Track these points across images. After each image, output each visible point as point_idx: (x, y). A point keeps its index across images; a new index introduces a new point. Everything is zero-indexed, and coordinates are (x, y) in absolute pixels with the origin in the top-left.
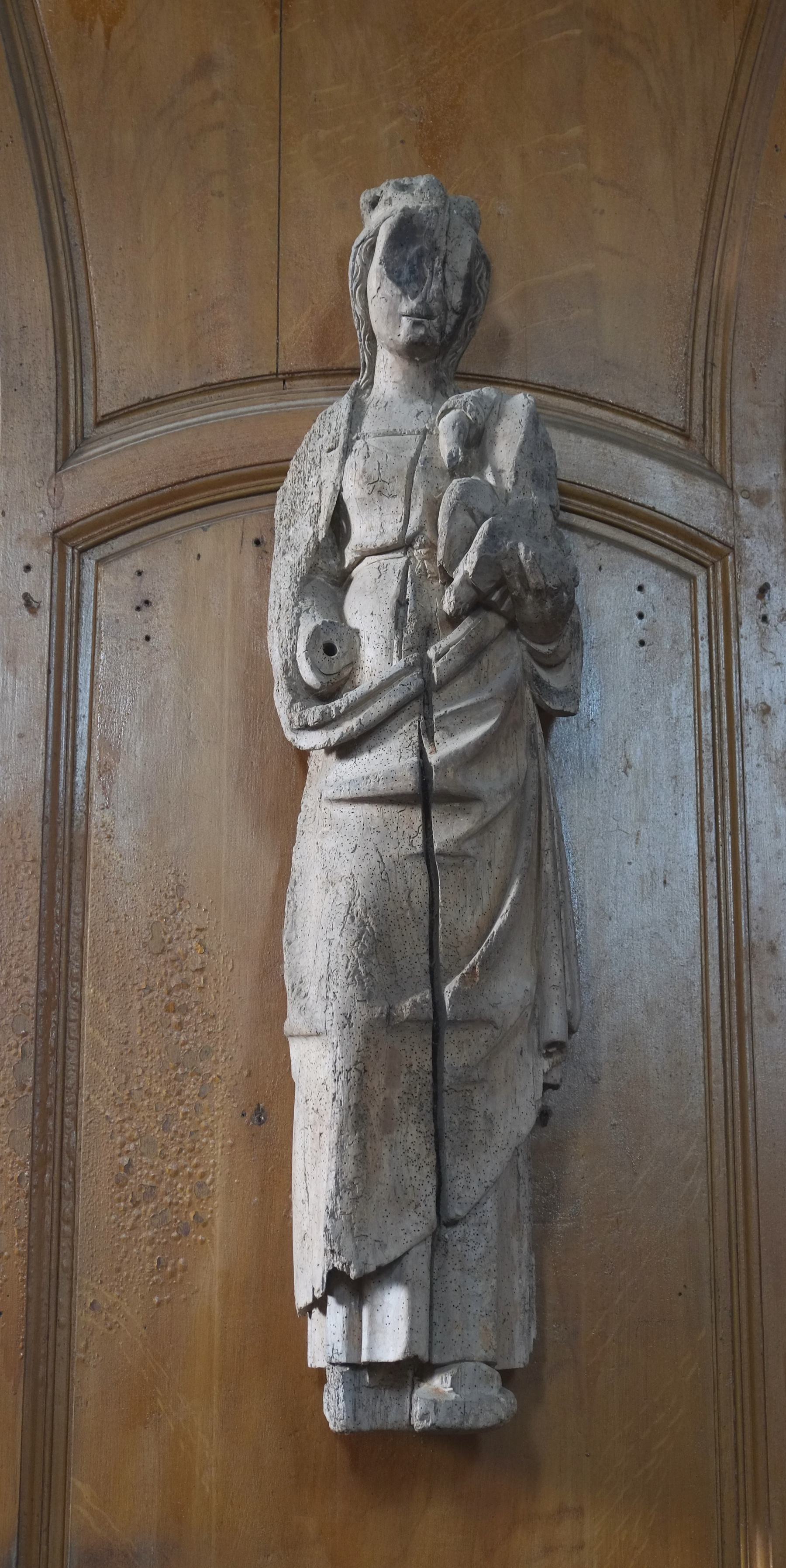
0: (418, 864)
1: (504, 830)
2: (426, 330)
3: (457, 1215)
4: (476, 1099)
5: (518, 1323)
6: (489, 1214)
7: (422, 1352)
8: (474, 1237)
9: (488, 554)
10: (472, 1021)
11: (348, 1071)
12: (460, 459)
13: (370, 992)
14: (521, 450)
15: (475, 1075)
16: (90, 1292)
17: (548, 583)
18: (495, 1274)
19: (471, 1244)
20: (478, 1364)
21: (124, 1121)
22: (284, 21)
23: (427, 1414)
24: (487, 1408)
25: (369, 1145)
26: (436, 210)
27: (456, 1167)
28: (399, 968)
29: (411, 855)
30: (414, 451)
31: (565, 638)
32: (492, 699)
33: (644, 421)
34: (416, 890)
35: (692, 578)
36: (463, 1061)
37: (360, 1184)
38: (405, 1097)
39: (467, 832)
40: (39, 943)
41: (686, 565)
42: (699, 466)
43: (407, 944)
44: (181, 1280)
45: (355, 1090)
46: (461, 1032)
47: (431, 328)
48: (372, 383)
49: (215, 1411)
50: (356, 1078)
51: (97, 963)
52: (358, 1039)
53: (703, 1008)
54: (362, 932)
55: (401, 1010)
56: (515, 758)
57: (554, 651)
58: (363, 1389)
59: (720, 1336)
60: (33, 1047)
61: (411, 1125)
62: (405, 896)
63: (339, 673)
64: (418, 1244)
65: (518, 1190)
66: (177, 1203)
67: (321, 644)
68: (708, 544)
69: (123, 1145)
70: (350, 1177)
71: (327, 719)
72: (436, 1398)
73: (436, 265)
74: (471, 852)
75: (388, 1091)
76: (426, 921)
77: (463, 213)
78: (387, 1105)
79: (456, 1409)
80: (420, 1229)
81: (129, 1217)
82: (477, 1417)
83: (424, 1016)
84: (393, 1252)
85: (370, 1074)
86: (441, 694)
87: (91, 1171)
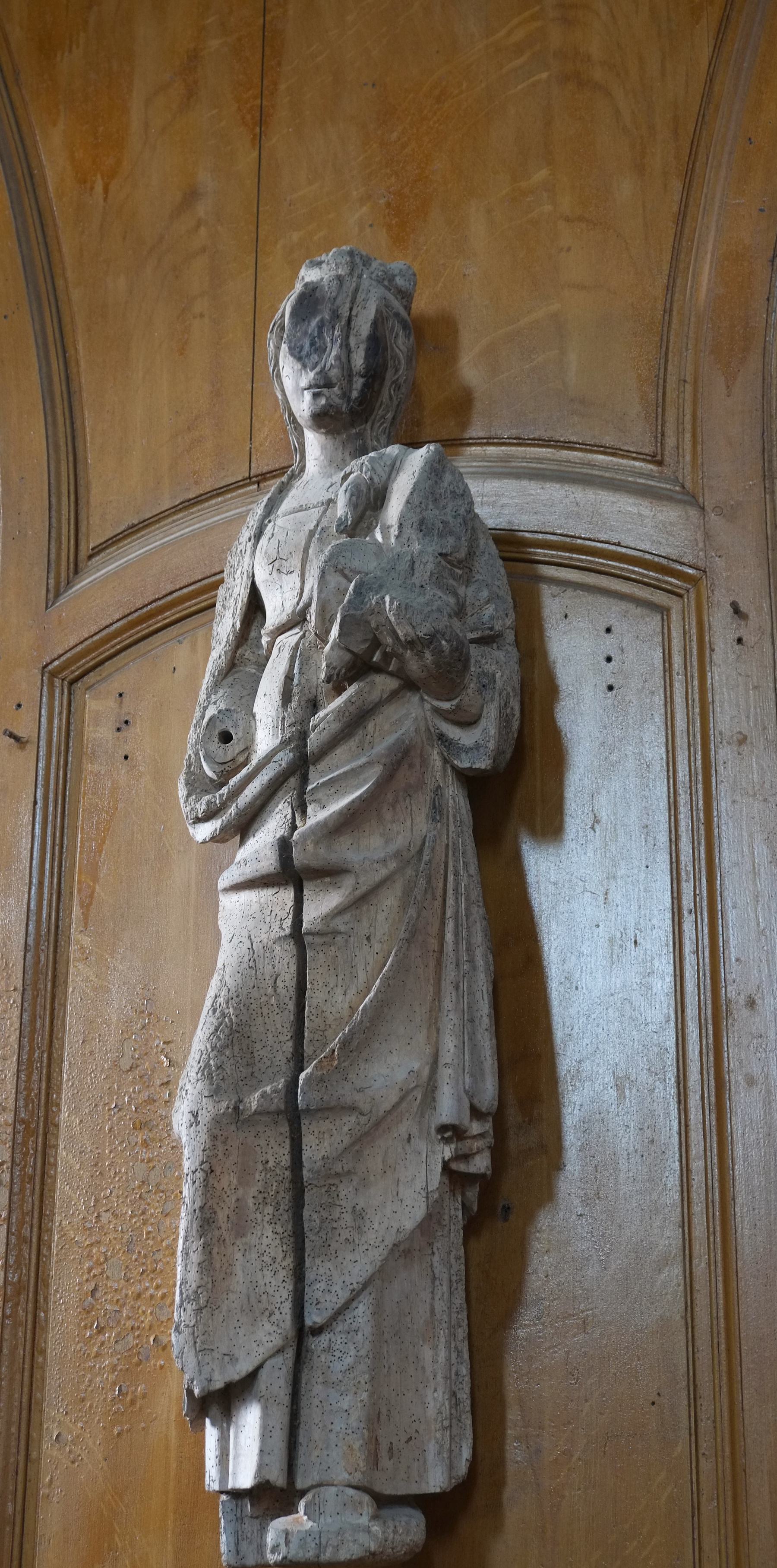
0: (286, 947)
1: (389, 900)
2: (327, 400)
3: (315, 1323)
4: (342, 1194)
5: (433, 1442)
6: (360, 1320)
7: (277, 1477)
8: (341, 1347)
9: (352, 612)
10: (330, 1109)
11: (194, 1172)
12: (349, 523)
13: (218, 1087)
14: (408, 502)
15: (338, 1168)
16: (56, 1424)
17: (418, 633)
18: (367, 1387)
19: (338, 1354)
20: (342, 1488)
21: (92, 1245)
22: (263, 137)
23: (278, 1546)
24: (350, 1538)
25: (215, 1250)
26: (339, 278)
27: (315, 1269)
28: (257, 1059)
29: (280, 938)
30: (315, 523)
31: (470, 691)
32: (369, 764)
33: (613, 455)
34: (283, 974)
35: (664, 611)
36: (323, 1153)
37: (205, 1293)
38: (260, 1196)
39: (336, 907)
40: (18, 1071)
41: (659, 598)
42: (670, 490)
43: (269, 1033)
44: (140, 1408)
45: (200, 1192)
46: (321, 1122)
47: (332, 396)
48: (304, 466)
49: (170, 1548)
50: (202, 1179)
51: (73, 1084)
52: (204, 1137)
53: (678, 1077)
54: (220, 1024)
55: (250, 1103)
56: (409, 823)
57: (457, 706)
58: (246, 1520)
59: (701, 1451)
60: (8, 1175)
61: (267, 1226)
62: (271, 982)
63: (233, 760)
64: (270, 1357)
65: (432, 1293)
66: (139, 1328)
67: (217, 733)
68: (679, 571)
69: (90, 1270)
70: (194, 1286)
71: (213, 807)
72: (289, 1528)
73: (336, 333)
74: (342, 928)
75: (240, 1192)
76: (291, 1006)
77: (374, 276)
78: (239, 1207)
79: (309, 1539)
80: (273, 1339)
81: (94, 1344)
82: (337, 1548)
83: (273, 1108)
84: (244, 1367)
85: (218, 1174)
86: (318, 766)
87: (61, 1298)
